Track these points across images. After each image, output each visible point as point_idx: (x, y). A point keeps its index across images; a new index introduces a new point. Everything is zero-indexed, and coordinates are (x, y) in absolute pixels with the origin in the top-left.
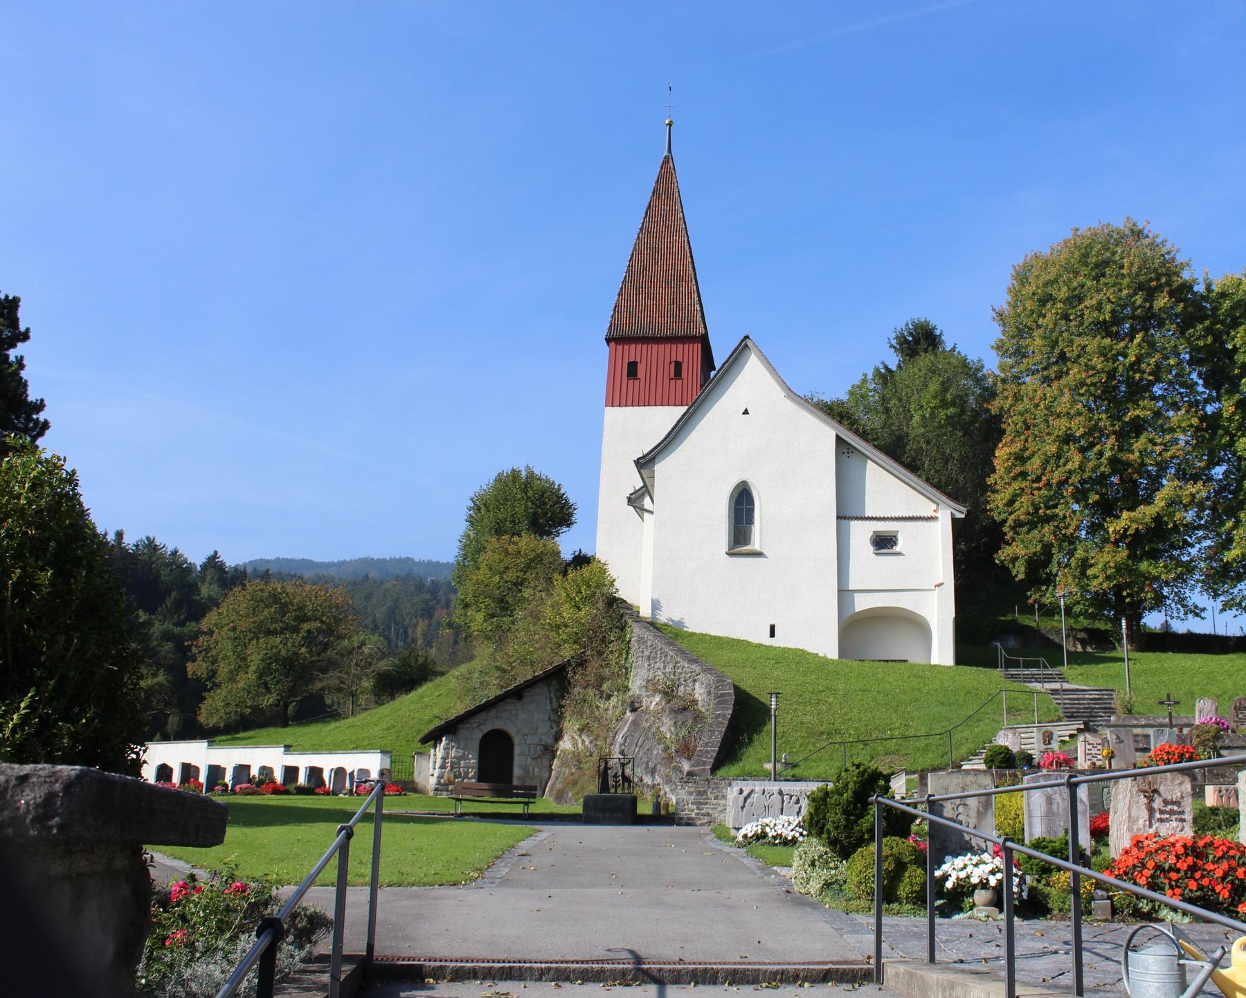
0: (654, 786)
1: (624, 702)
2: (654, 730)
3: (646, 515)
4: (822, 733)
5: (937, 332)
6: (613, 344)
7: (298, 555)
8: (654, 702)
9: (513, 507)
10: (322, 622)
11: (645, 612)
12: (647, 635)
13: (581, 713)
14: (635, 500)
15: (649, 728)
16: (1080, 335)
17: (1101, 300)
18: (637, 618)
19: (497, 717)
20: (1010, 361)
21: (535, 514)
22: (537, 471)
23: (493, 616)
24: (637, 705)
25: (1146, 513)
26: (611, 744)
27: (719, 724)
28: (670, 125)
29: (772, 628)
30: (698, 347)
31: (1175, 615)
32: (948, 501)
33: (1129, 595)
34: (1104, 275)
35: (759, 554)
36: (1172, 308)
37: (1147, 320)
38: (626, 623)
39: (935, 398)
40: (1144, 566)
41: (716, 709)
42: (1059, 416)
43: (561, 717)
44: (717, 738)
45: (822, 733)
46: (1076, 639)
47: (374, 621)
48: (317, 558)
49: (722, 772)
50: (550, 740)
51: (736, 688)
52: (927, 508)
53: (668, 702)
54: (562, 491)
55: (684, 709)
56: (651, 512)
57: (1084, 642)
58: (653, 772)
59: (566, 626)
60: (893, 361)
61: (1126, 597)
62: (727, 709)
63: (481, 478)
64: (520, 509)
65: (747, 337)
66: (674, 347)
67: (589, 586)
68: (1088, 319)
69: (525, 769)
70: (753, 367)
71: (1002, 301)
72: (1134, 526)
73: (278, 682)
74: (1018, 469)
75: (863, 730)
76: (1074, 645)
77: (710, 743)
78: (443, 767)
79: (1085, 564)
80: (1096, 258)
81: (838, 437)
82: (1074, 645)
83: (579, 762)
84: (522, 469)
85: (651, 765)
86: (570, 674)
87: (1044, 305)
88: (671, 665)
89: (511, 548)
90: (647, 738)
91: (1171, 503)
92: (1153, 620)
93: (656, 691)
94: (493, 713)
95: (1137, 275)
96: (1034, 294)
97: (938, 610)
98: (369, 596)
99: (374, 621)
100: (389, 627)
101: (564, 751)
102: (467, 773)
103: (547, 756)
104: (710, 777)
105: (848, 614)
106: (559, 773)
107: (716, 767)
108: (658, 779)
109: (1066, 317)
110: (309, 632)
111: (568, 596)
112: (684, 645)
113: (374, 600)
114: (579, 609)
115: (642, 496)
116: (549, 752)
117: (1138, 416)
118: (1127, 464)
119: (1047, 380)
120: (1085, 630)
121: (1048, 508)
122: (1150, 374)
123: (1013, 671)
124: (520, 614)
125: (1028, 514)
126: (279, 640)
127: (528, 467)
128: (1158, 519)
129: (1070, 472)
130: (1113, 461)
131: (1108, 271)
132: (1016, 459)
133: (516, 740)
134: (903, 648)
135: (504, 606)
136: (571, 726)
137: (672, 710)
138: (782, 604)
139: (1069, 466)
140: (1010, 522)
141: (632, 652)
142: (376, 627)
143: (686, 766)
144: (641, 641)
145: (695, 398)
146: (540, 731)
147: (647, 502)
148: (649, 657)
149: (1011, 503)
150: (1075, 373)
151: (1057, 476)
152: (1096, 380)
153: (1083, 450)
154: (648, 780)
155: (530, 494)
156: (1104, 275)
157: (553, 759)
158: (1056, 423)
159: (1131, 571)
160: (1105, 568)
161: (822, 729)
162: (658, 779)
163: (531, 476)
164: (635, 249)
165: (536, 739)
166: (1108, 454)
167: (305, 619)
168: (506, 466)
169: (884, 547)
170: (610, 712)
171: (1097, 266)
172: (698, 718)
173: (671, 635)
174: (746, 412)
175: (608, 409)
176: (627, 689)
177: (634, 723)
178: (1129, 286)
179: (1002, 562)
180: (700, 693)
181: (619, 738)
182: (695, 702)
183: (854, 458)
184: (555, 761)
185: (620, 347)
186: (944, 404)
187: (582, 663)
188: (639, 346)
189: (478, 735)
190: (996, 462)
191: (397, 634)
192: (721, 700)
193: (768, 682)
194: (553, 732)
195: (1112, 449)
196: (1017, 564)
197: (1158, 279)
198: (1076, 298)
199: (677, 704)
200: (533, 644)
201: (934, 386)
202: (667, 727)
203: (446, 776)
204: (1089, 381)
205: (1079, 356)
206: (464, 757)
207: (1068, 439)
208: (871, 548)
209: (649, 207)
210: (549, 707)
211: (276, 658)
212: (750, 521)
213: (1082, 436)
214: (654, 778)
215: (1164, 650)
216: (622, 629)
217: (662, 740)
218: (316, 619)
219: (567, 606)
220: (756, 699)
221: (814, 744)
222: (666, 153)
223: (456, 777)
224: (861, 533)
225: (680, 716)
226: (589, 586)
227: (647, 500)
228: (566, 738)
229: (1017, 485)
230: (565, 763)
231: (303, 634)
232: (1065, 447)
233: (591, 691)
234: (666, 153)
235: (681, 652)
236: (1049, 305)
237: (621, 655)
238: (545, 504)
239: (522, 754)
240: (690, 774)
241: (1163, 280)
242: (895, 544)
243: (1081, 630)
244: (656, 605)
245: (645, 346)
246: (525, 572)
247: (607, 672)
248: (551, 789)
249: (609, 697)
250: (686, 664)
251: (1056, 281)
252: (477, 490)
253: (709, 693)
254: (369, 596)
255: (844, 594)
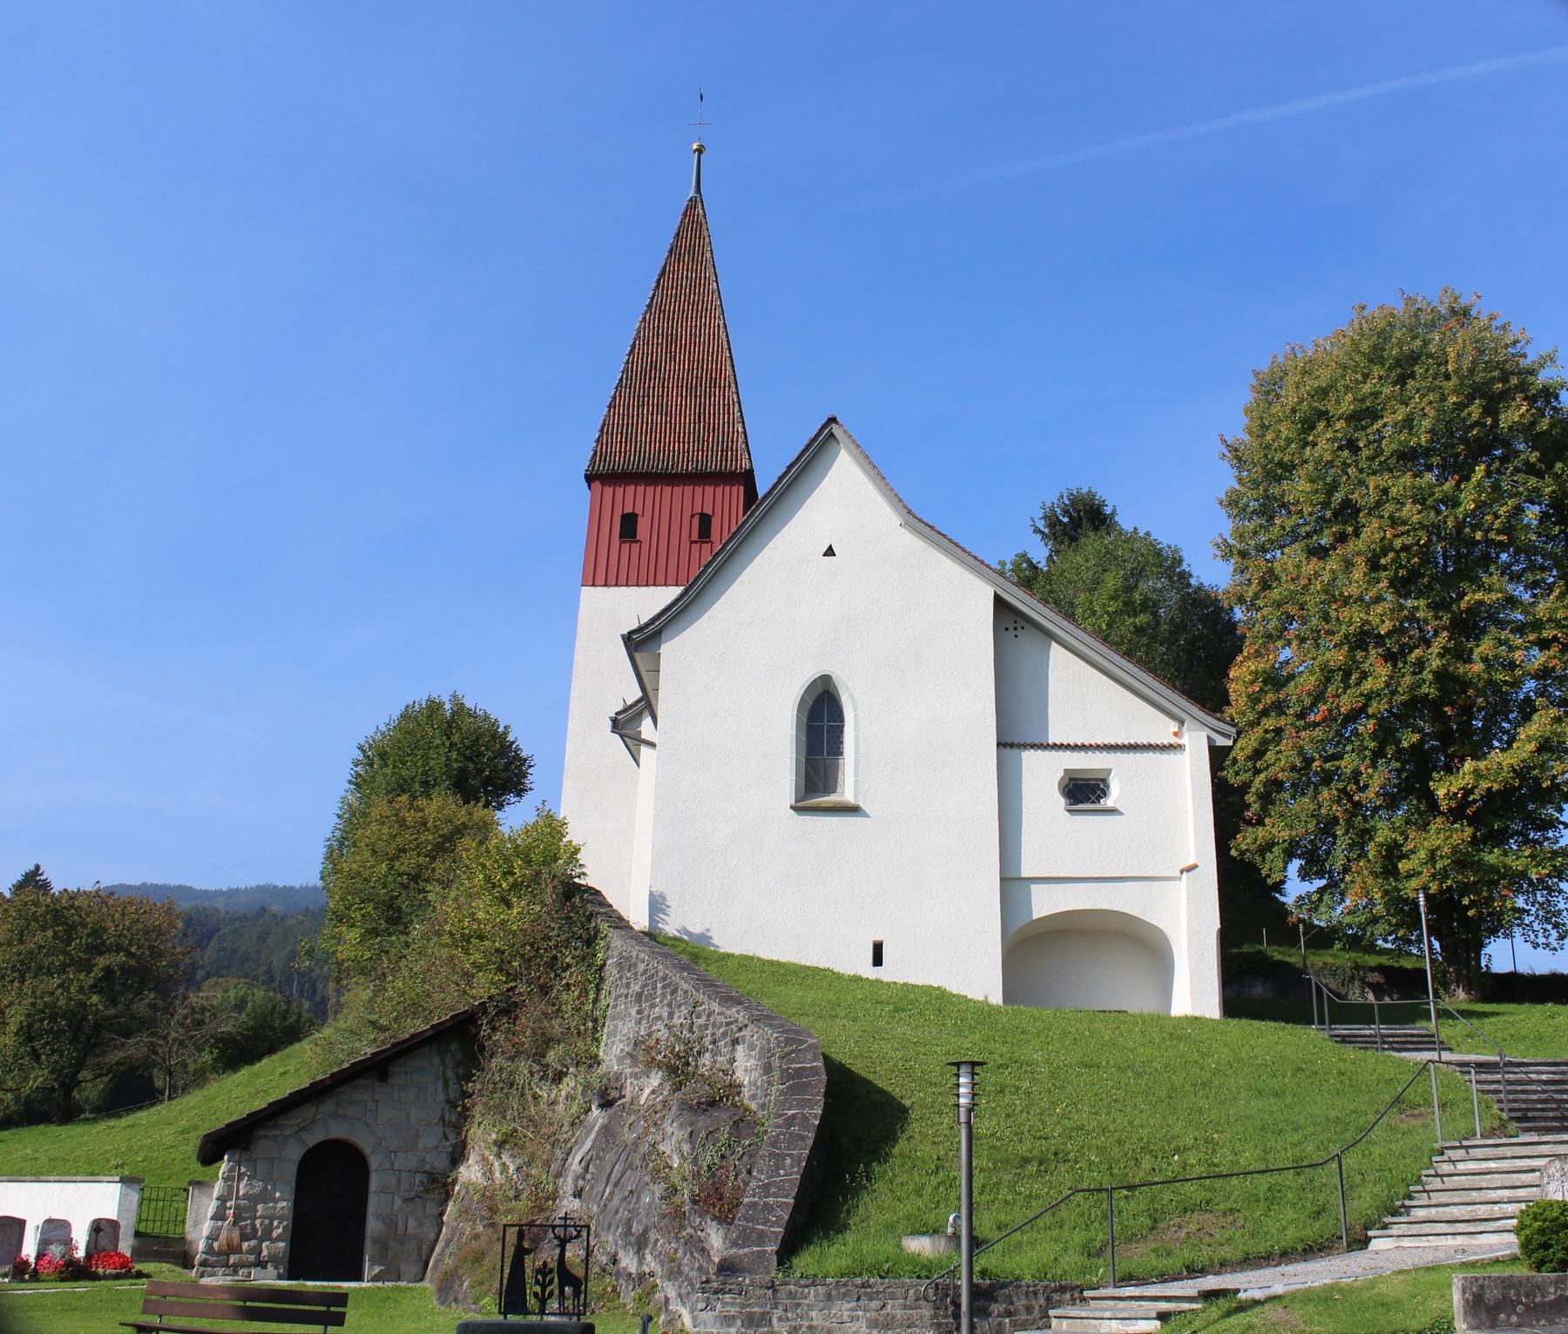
0: (642, 1277)
1: (587, 1087)
2: (644, 1148)
3: (644, 749)
4: (1026, 1161)
5: (1108, 510)
6: (597, 485)
7: (173, 880)
8: (649, 1087)
9: (426, 758)
10: (131, 955)
11: (639, 918)
12: (635, 951)
13: (501, 1109)
14: (626, 724)
15: (636, 1144)
16: (1374, 473)
17: (1415, 415)
18: (620, 923)
19: (336, 1116)
20: (1250, 526)
21: (462, 771)
22: (469, 704)
23: (374, 932)
24: (614, 1094)
25: (1502, 761)
26: (558, 1175)
27: (794, 1139)
28: (700, 151)
29: (878, 949)
30: (739, 492)
31: (1541, 940)
32: (1201, 715)
33: (1473, 904)
34: (1412, 376)
35: (852, 810)
36: (1533, 423)
37: (1486, 445)
38: (597, 930)
39: (1114, 598)
40: (1492, 857)
41: (784, 1105)
42: (1346, 601)
43: (465, 1116)
44: (791, 1174)
45: (1026, 1161)
46: (1364, 982)
47: (269, 971)
48: (199, 885)
49: (805, 1261)
50: (441, 1163)
51: (826, 1058)
52: (1160, 728)
53: (678, 1087)
54: (511, 738)
55: (712, 1103)
56: (652, 745)
57: (1378, 990)
58: (640, 1244)
59: (482, 938)
60: (1040, 553)
61: (1468, 908)
62: (811, 1104)
63: (375, 713)
64: (437, 762)
65: (833, 420)
66: (699, 490)
67: (529, 862)
68: (1388, 447)
69: (390, 1222)
70: (844, 476)
71: (1238, 429)
72: (1484, 785)
73: (53, 1051)
74: (1270, 698)
75: (1116, 1152)
76: (1363, 994)
77: (774, 1185)
78: (219, 1216)
79: (1393, 853)
80: (1398, 354)
81: (999, 602)
82: (1363, 994)
83: (493, 1210)
84: (446, 699)
85: (637, 1228)
86: (485, 1031)
87: (1312, 427)
88: (684, 1011)
89: (410, 817)
90: (630, 1166)
91: (1545, 746)
92: (1500, 955)
93: (651, 1064)
94: (328, 1107)
95: (1472, 371)
96: (1294, 411)
97: (1189, 921)
98: (263, 938)
99: (269, 971)
100: (289, 980)
101: (466, 1187)
102: (269, 1230)
103: (436, 1195)
104: (774, 1273)
105: (1019, 922)
106: (453, 1231)
107: (789, 1249)
108: (651, 1264)
109: (1352, 445)
110: (108, 971)
111: (488, 879)
112: (713, 972)
113: (270, 942)
114: (509, 905)
115: (638, 717)
116: (439, 1185)
117: (1481, 603)
118: (1464, 684)
119: (1321, 553)
120: (1380, 969)
121: (1326, 760)
122: (1499, 532)
123: (1342, 1030)
124: (417, 929)
125: (1293, 768)
126: (56, 981)
127: (455, 696)
128: (1521, 772)
129: (1369, 697)
130: (1442, 676)
131: (1418, 370)
132: (1265, 682)
133: (374, 1162)
134: (1120, 990)
135: (394, 918)
136: (482, 1133)
137: (685, 1107)
138: (895, 901)
139: (1368, 685)
140: (1258, 783)
141: (606, 987)
142: (271, 979)
143: (716, 1239)
144: (626, 964)
145: (734, 529)
146: (421, 1145)
147: (646, 728)
148: (639, 996)
149: (1258, 754)
150: (1373, 531)
151: (1346, 703)
152: (1409, 540)
153: (1390, 657)
154: (628, 1262)
155: (456, 738)
156: (1412, 376)
157: (446, 1200)
158: (1345, 614)
159: (1478, 866)
160: (1432, 856)
161: (1023, 1150)
162: (651, 1264)
163: (459, 709)
164: (638, 337)
165: (413, 1162)
166: (1436, 663)
167: (98, 949)
168: (418, 695)
169: (1087, 800)
170: (560, 1108)
171: (1398, 363)
172: (743, 1123)
173: (691, 958)
174: (830, 552)
175: (587, 592)
176: (595, 1061)
177: (607, 1131)
178: (1455, 392)
179: (1242, 853)
180: (745, 1067)
181: (575, 1164)
182: (735, 1088)
183: (1027, 639)
184: (451, 1203)
185: (609, 490)
186: (1130, 608)
187: (508, 1009)
188: (641, 489)
189: (295, 1152)
190: (1232, 687)
191: (302, 991)
192: (795, 1082)
193: (887, 1047)
194: (447, 1146)
195: (1441, 656)
196: (1269, 856)
197: (1505, 380)
198: (1365, 415)
199: (695, 1091)
200: (432, 979)
201: (1111, 581)
202: (673, 1143)
203: (223, 1235)
204: (1398, 543)
205: (1378, 504)
206: (263, 1197)
207: (1362, 639)
208: (1061, 801)
209: (663, 273)
210: (441, 1098)
211: (52, 1013)
212: (836, 749)
213: (1390, 634)
214: (641, 1260)
215: (1541, 1000)
216: (590, 942)
217: (660, 1171)
218: (119, 948)
219: (488, 899)
220: (869, 1083)
221: (1012, 1188)
222: (692, 193)
223: (244, 1237)
224: (1042, 775)
225: (703, 1122)
226: (529, 862)
227: (647, 722)
228: (473, 1158)
229: (1270, 723)
230: (464, 1212)
231: (97, 973)
232: (1359, 655)
233: (524, 1066)
234: (692, 193)
235: (707, 984)
236: (1321, 426)
237: (585, 992)
238: (480, 754)
239: (384, 1190)
240: (728, 1268)
241: (1514, 381)
242: (1104, 793)
243: (1372, 969)
244: (657, 905)
245: (650, 489)
246: (434, 859)
247: (556, 1027)
248: (436, 1267)
249: (559, 1077)
250: (715, 1007)
251: (1332, 386)
252: (371, 732)
253: (768, 1069)
254: (263, 938)
255: (1012, 885)
